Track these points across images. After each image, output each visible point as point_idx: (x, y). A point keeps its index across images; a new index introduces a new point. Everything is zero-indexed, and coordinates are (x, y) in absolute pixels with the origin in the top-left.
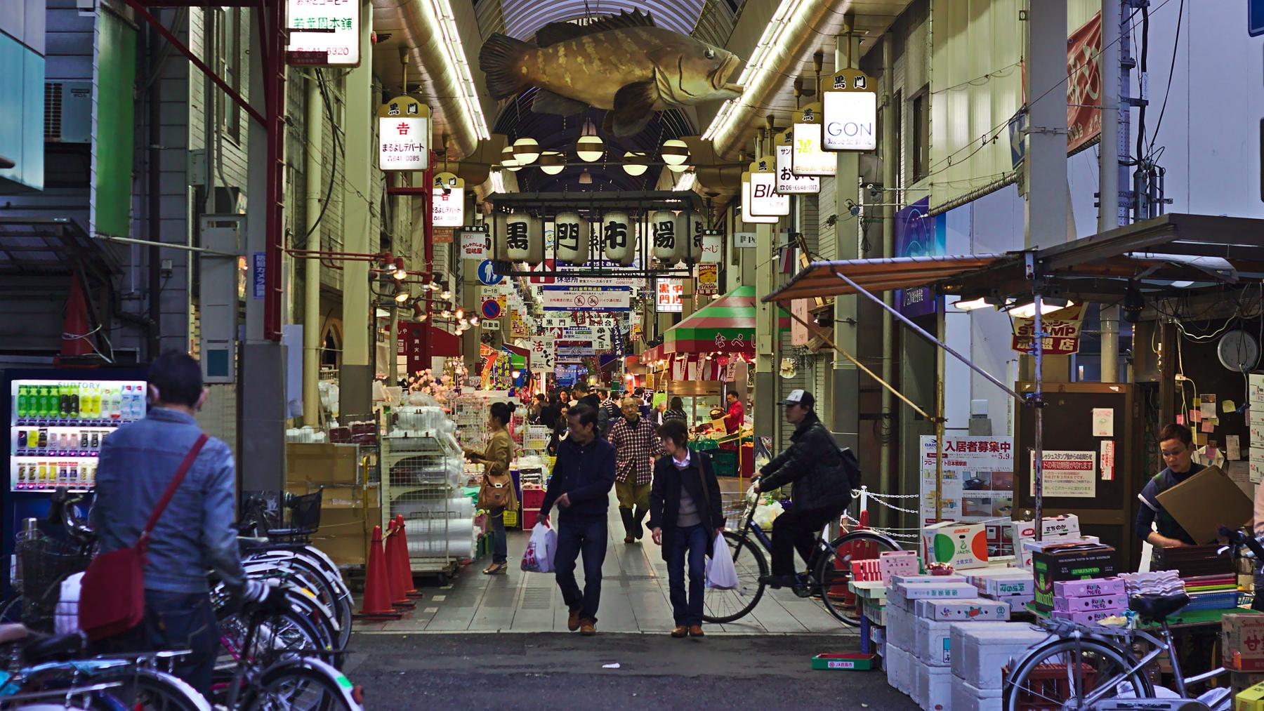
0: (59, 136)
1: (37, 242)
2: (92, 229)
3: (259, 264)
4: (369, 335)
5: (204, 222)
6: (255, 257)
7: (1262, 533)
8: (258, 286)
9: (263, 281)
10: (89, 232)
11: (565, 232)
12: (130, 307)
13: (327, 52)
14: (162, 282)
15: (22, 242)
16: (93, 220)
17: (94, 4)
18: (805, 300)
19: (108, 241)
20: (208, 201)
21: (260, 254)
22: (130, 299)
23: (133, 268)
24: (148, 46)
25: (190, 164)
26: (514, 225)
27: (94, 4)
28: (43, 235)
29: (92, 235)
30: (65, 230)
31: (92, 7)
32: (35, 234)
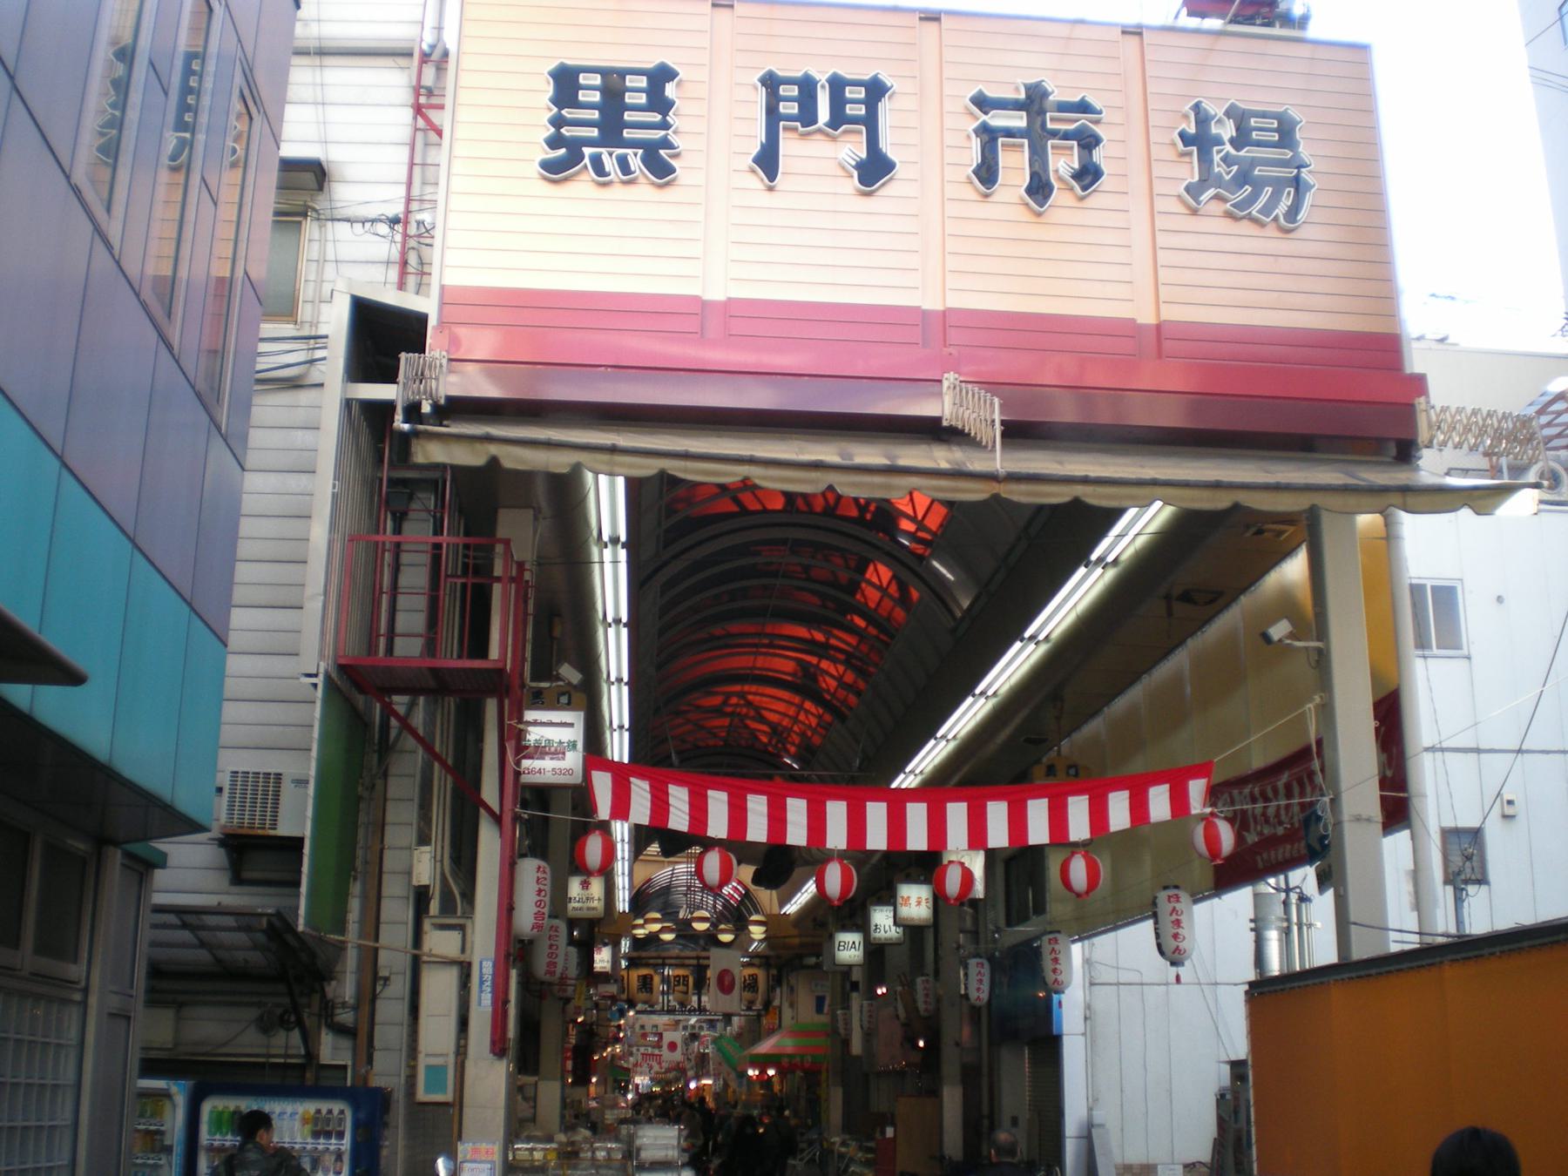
0: (275, 829)
1: (241, 938)
2: (301, 921)
3: (484, 970)
4: (455, 1076)
5: (427, 925)
6: (481, 963)
7: (882, 1156)
8: (483, 995)
9: (489, 989)
10: (297, 926)
11: (679, 981)
12: (345, 1017)
13: (888, 89)
14: (379, 989)
15: (224, 937)
16: (302, 911)
17: (318, 669)
18: (1395, 948)
19: (320, 939)
20: (432, 902)
21: (487, 960)
22: (344, 1008)
23: (348, 974)
24: (376, 741)
25: (415, 861)
26: (645, 977)
27: (318, 669)
28: (248, 929)
29: (301, 928)
30: (270, 923)
31: (315, 672)
32: (239, 929)
